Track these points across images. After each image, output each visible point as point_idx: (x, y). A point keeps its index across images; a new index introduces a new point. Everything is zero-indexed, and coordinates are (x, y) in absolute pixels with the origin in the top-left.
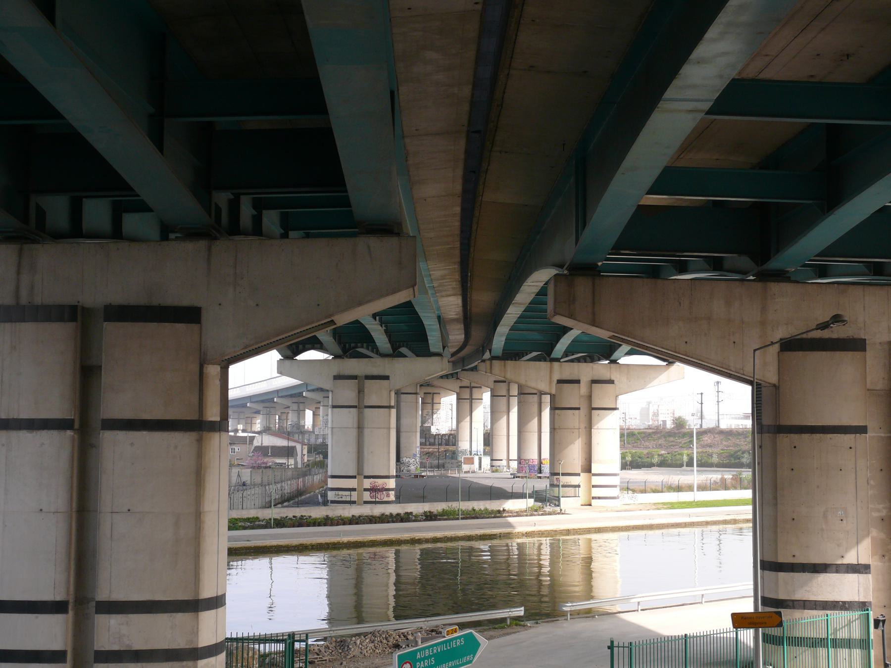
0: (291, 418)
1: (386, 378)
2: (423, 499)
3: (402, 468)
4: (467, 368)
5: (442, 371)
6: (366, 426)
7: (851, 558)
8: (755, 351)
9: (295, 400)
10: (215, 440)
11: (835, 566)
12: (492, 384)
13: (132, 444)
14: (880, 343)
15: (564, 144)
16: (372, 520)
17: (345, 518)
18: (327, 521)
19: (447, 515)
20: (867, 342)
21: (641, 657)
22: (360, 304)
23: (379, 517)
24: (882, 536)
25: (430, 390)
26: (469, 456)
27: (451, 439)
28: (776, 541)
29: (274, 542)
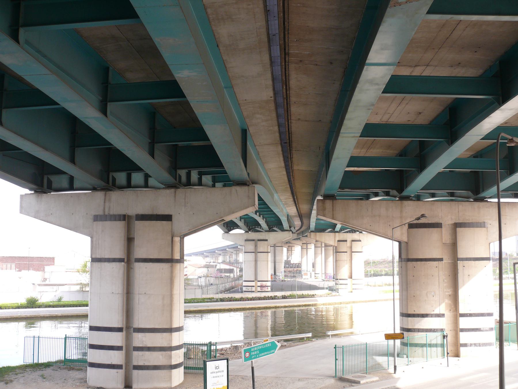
0: (234, 256)
1: (267, 240)
2: (282, 290)
3: (277, 278)
4: (303, 236)
5: (289, 237)
6: (258, 260)
7: (437, 312)
8: (393, 229)
9: (235, 249)
10: (178, 266)
11: (431, 315)
12: (315, 242)
13: (146, 268)
14: (448, 224)
15: (319, 147)
16: (260, 299)
17: (249, 298)
18: (241, 299)
19: (294, 297)
20: (442, 224)
21: (355, 352)
22: (233, 213)
23: (263, 298)
24: (450, 302)
25: (291, 245)
26: (306, 272)
27: (299, 266)
28: (407, 306)
29: (219, 308)
